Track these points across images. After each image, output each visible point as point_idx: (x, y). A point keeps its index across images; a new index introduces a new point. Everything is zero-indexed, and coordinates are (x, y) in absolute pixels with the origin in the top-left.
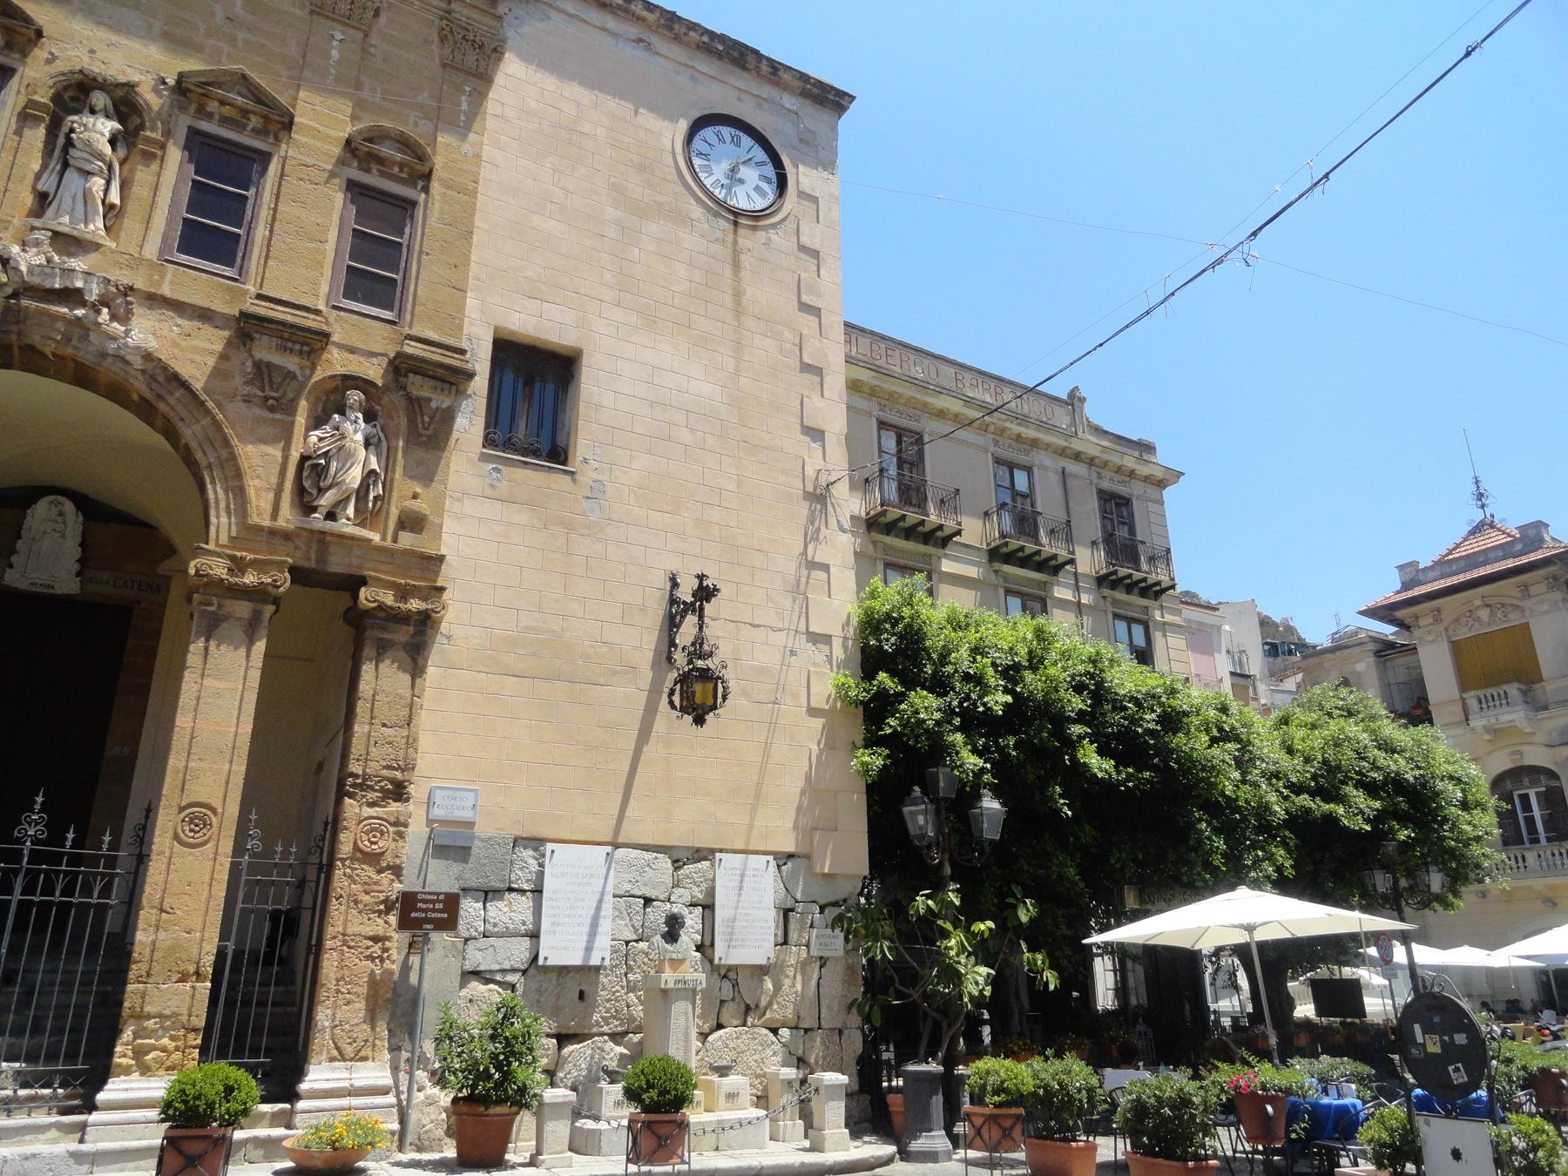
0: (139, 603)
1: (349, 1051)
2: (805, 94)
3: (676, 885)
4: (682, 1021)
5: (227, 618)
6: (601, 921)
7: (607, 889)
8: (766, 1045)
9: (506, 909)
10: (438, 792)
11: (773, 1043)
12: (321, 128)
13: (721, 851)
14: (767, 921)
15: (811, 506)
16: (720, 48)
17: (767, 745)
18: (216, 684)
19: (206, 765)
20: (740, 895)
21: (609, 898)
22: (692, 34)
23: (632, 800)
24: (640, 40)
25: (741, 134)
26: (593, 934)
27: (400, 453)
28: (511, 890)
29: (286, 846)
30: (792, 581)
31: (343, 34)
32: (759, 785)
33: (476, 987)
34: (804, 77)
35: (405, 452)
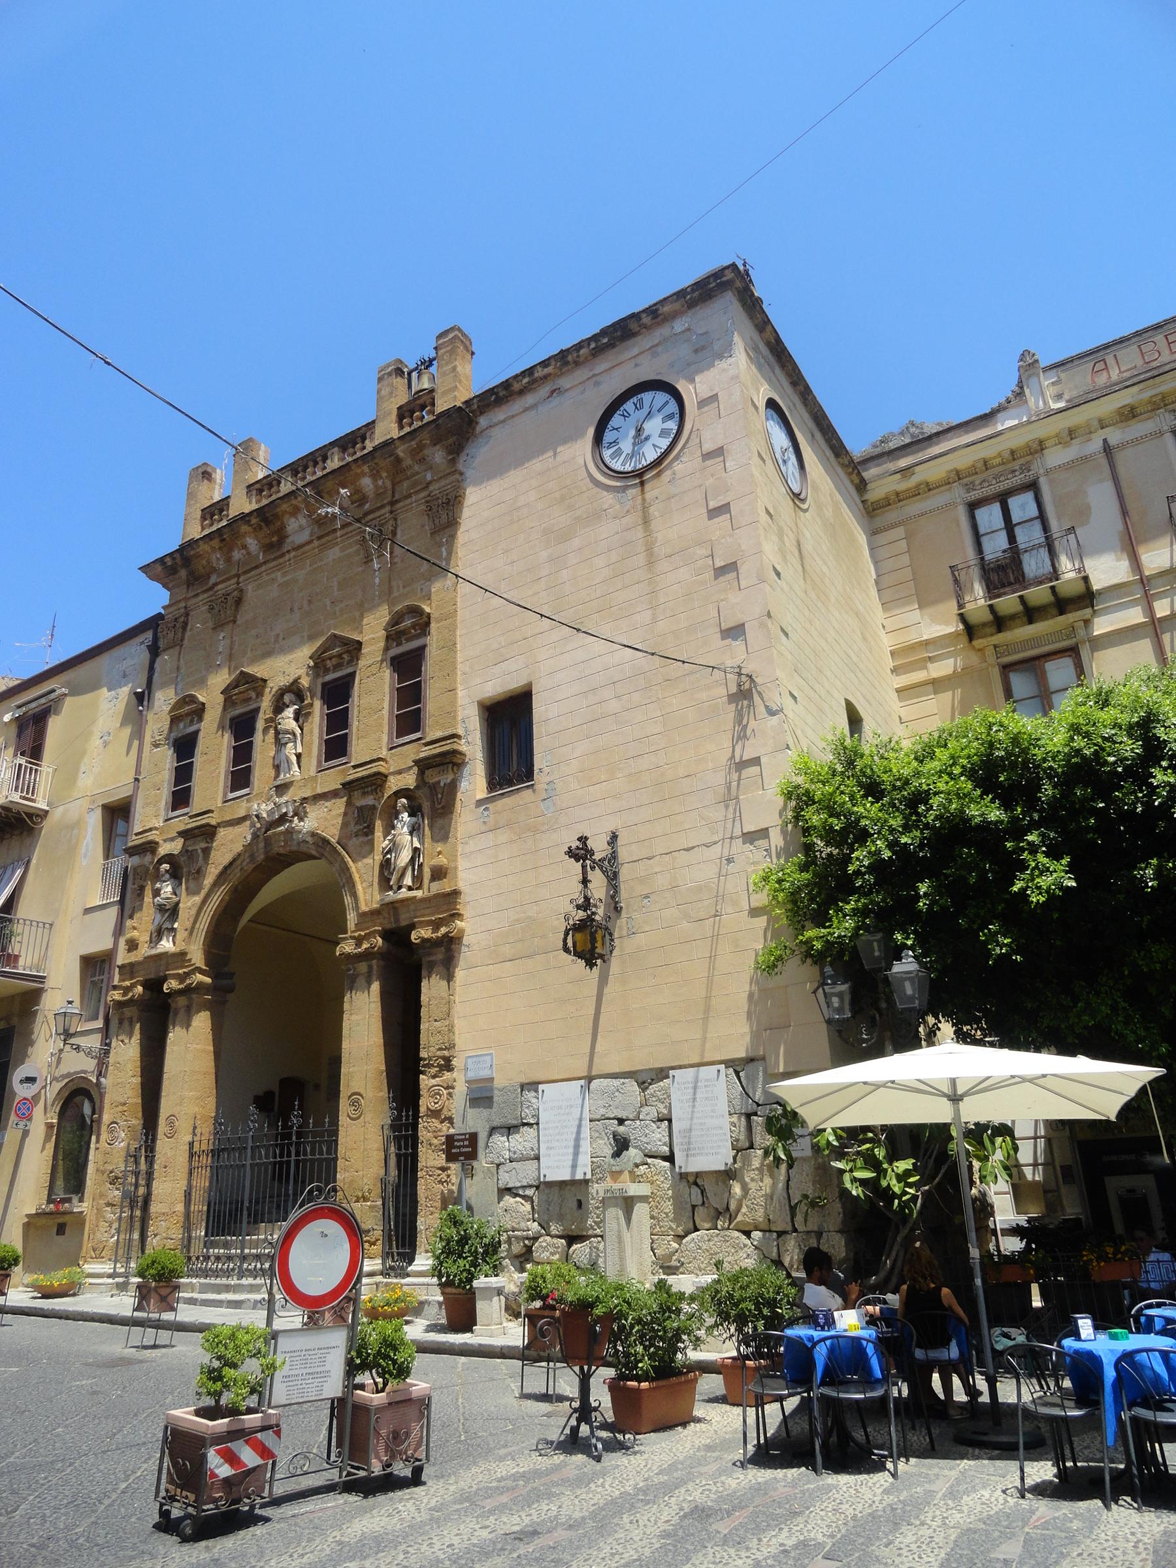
2: (691, 305)
3: (645, 1103)
4: (615, 1226)
5: (358, 975)
6: (582, 1143)
7: (584, 1116)
8: (739, 1247)
9: (520, 1140)
11: (745, 1246)
13: (673, 1068)
14: (721, 1128)
15: (737, 705)
16: (605, 340)
17: (712, 958)
19: (355, 1069)
20: (694, 1106)
21: (586, 1123)
22: (582, 352)
23: (599, 1037)
24: (553, 391)
26: (576, 1154)
27: (427, 828)
28: (525, 1124)
29: (407, 1112)
30: (722, 790)
32: (708, 998)
33: (509, 1200)
34: (680, 294)
35: (431, 827)
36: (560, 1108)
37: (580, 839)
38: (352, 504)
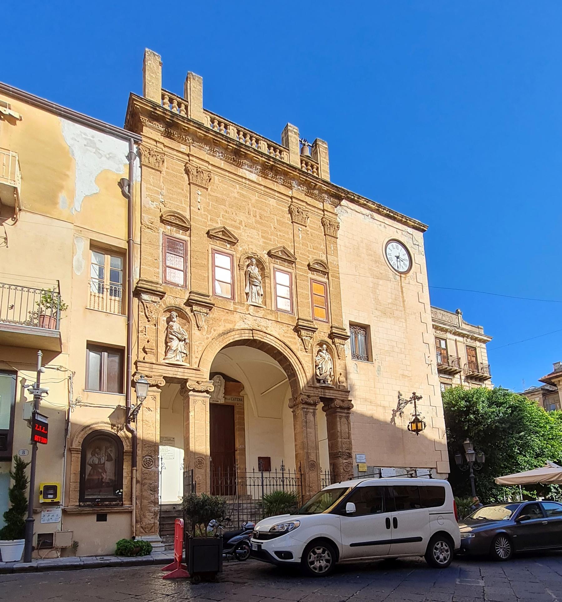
12: (302, 262)
18: (310, 430)
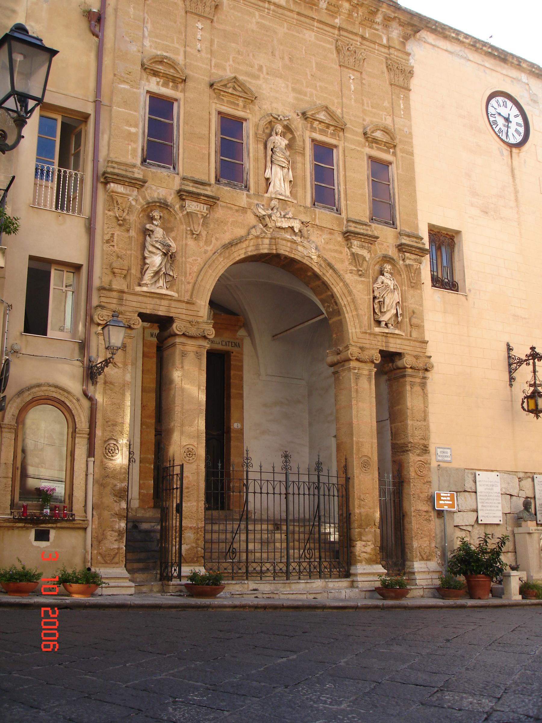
0: (232, 352)
1: (425, 556)
10: (438, 449)
16: (496, 54)
25: (507, 100)
28: (465, 491)
31: (353, 75)
34: (532, 65)
36: (487, 485)
37: (531, 348)
38: (326, 9)
